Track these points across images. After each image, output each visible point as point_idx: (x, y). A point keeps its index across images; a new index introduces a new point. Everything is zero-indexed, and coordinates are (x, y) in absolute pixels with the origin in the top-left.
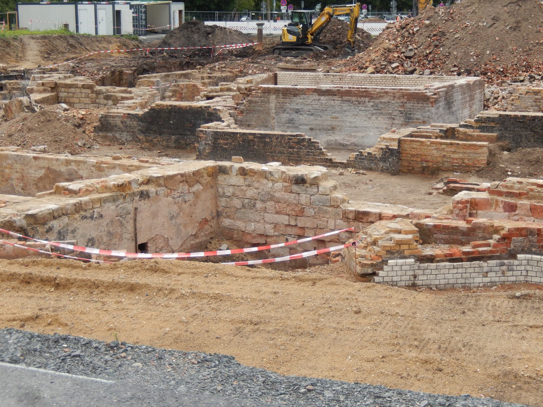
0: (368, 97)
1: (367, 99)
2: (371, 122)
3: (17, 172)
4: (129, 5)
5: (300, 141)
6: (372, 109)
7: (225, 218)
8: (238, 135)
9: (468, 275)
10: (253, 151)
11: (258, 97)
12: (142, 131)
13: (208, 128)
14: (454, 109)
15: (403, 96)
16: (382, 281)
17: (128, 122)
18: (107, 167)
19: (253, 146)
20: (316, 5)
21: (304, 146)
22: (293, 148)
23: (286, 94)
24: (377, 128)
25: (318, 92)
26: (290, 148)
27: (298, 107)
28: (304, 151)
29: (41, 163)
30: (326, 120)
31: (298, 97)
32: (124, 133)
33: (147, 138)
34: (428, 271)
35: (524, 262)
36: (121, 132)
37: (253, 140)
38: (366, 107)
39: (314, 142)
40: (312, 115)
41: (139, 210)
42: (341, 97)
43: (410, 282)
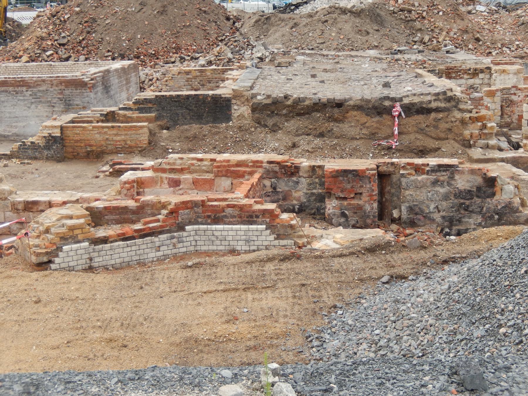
0: (26, 86)
1: (24, 89)
2: (31, 111)
9: (142, 251)
14: (112, 93)
15: (61, 84)
16: (58, 267)
24: (37, 116)
35: (193, 233)
38: (24, 96)
43: (87, 266)
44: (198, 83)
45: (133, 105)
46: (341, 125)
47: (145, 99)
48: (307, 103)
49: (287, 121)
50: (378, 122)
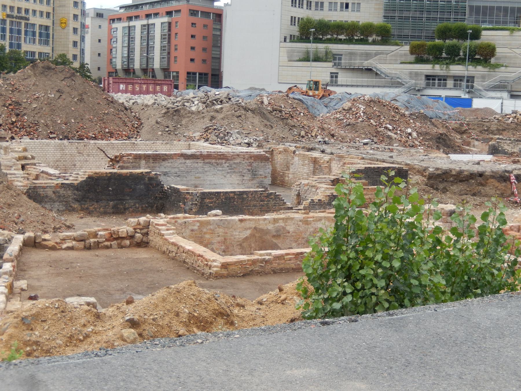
0: (225, 159)
1: (224, 161)
2: (226, 179)
3: (219, 236)
6: (228, 168)
8: (222, 194)
10: (233, 207)
11: (129, 163)
12: (77, 200)
15: (251, 158)
17: (62, 191)
18: (313, 221)
21: (271, 198)
22: (263, 201)
23: (156, 159)
24: (231, 184)
25: (184, 157)
26: (261, 201)
27: (166, 171)
28: (272, 202)
29: (247, 224)
30: (191, 180)
31: (167, 162)
32: (55, 203)
33: (83, 206)
36: (52, 203)
37: (233, 198)
38: (223, 167)
39: (278, 195)
40: (178, 176)
42: (204, 160)
46: (485, 188)
47: (358, 170)
48: (466, 173)
49: (452, 185)
50: (505, 186)
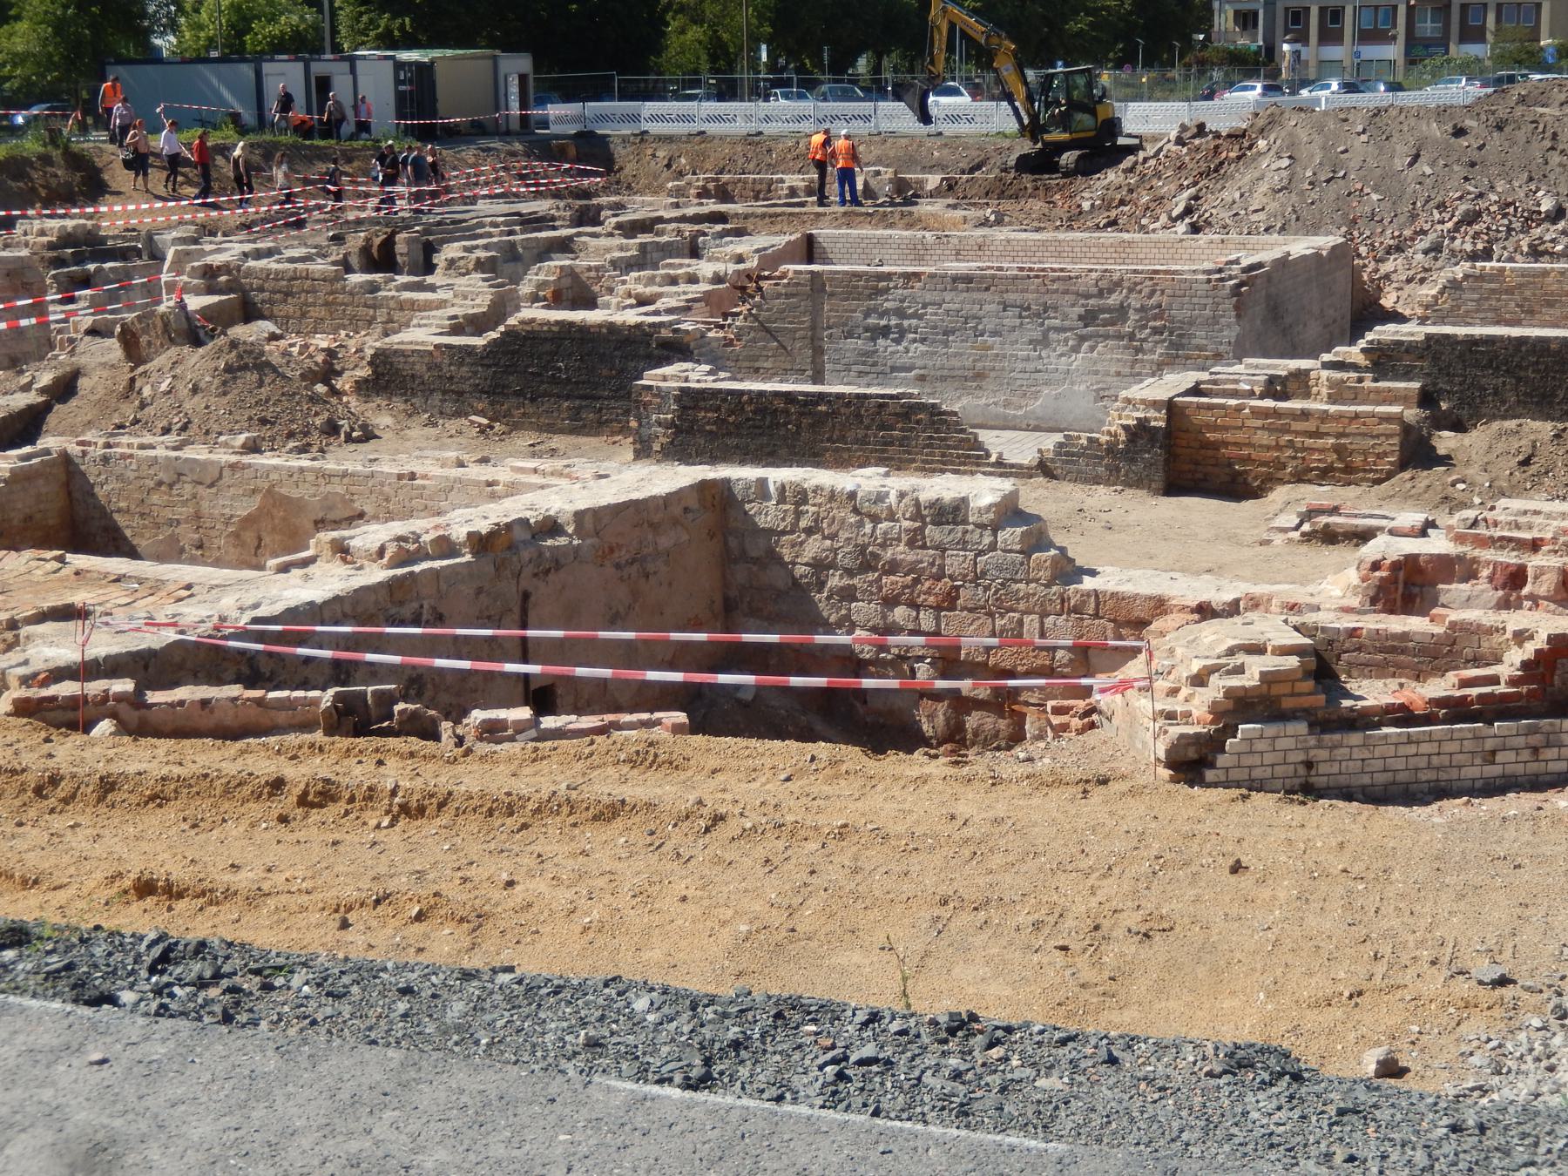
4: (391, 62)
5: (909, 412)
7: (745, 615)
8: (745, 398)
9: (1445, 760)
13: (665, 379)
14: (1288, 320)
16: (1223, 778)
19: (785, 424)
20: (860, 55)
21: (918, 422)
34: (1342, 751)
41: (532, 599)
43: (1297, 781)
44: (1517, 306)
45: (1362, 356)
